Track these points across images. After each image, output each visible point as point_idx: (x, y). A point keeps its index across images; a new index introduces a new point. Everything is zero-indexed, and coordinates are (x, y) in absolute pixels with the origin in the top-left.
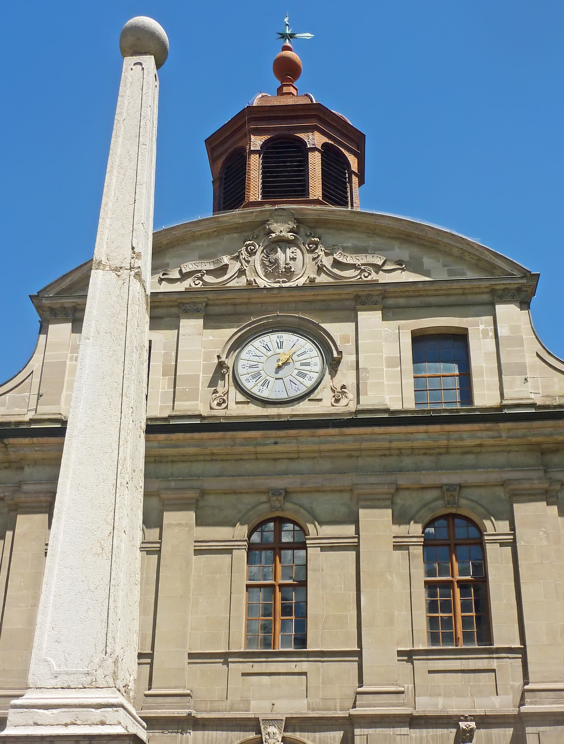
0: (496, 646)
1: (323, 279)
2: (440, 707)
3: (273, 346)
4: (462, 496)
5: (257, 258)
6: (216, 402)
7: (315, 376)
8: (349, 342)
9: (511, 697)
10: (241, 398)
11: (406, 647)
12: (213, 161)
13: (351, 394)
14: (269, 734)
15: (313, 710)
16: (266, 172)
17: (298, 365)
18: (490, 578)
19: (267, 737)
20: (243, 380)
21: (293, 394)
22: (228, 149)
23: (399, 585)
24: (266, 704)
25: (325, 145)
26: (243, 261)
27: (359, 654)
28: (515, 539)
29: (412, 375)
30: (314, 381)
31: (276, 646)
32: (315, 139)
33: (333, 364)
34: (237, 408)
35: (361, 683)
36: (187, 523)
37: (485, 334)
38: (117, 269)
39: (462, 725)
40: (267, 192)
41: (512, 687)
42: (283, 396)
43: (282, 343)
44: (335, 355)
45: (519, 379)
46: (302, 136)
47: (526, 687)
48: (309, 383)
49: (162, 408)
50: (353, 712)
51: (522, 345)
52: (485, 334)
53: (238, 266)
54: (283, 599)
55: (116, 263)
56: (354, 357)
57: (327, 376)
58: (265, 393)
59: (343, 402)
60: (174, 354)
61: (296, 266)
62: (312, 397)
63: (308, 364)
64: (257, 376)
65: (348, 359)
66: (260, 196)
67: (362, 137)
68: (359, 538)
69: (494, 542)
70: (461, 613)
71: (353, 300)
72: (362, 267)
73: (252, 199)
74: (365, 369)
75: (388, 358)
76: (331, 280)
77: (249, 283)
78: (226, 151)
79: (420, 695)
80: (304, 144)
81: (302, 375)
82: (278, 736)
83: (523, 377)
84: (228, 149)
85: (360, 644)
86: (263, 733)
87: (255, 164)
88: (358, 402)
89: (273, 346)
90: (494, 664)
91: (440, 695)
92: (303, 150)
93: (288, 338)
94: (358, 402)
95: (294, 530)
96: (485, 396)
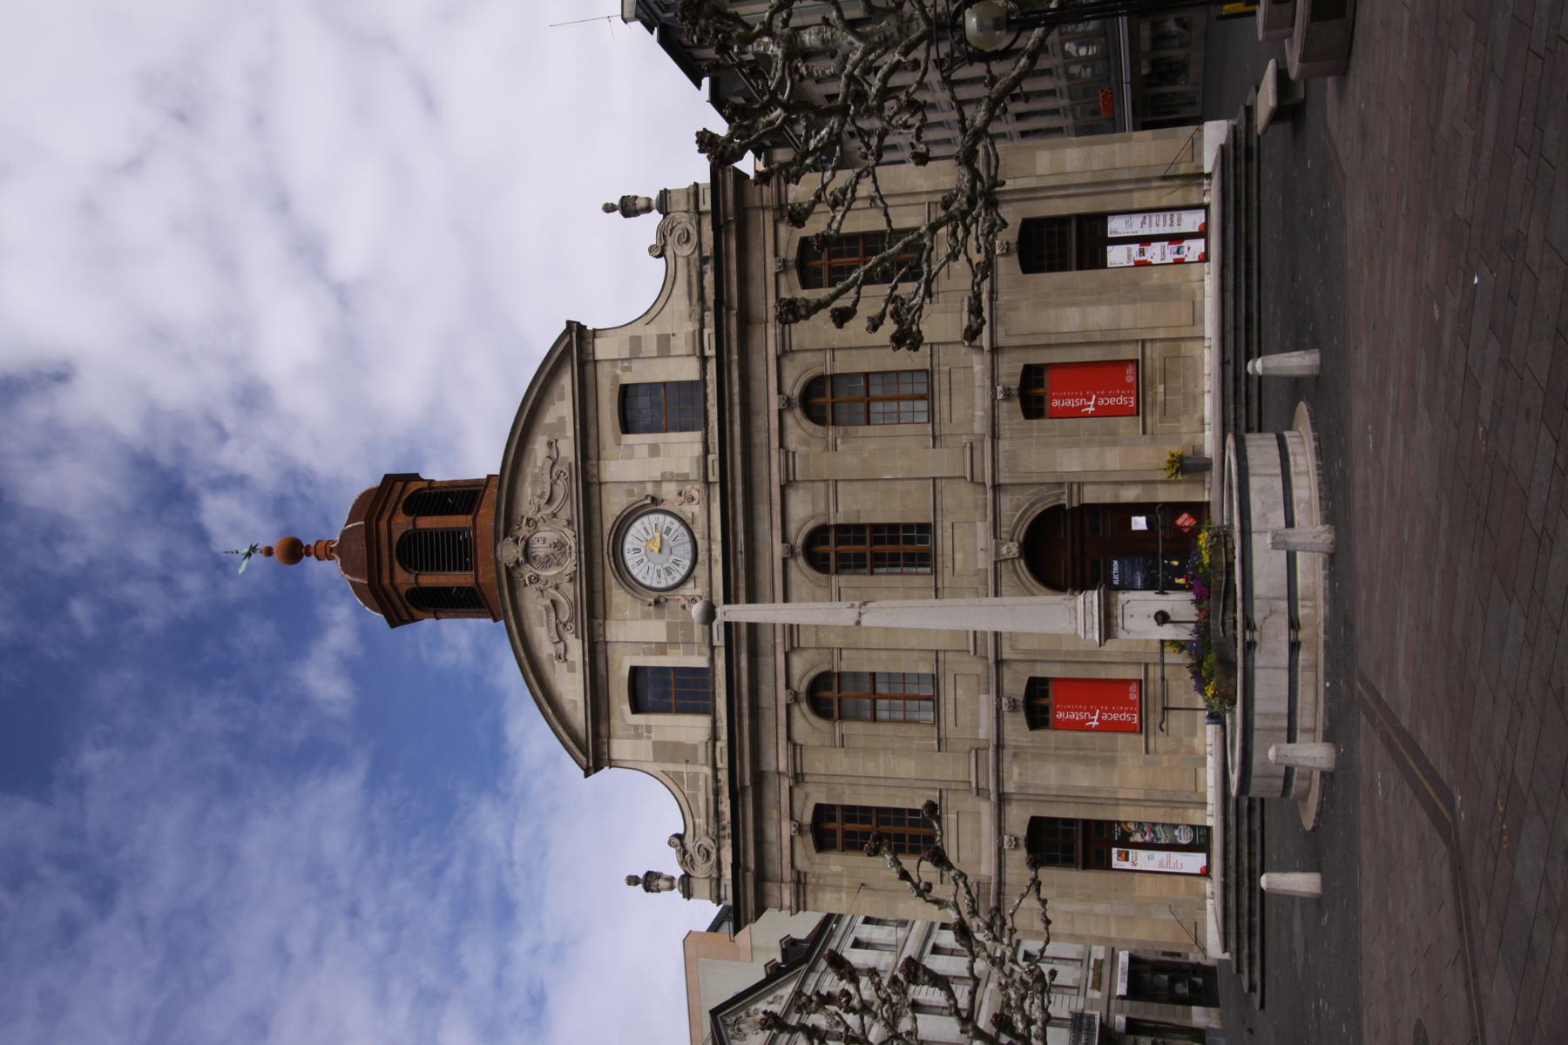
3: (638, 557)
4: (1192, 626)
5: (544, 574)
7: (669, 519)
10: (690, 585)
16: (440, 567)
21: (687, 538)
27: (1144, 341)
32: (402, 523)
33: (654, 504)
37: (629, 369)
38: (1044, 902)
39: (1000, 396)
42: (689, 547)
46: (396, 536)
51: (639, 338)
53: (552, 591)
55: (1038, 905)
58: (687, 563)
59: (695, 494)
61: (552, 537)
64: (668, 571)
71: (588, 485)
76: (608, 525)
77: (571, 580)
87: (429, 580)
89: (638, 557)
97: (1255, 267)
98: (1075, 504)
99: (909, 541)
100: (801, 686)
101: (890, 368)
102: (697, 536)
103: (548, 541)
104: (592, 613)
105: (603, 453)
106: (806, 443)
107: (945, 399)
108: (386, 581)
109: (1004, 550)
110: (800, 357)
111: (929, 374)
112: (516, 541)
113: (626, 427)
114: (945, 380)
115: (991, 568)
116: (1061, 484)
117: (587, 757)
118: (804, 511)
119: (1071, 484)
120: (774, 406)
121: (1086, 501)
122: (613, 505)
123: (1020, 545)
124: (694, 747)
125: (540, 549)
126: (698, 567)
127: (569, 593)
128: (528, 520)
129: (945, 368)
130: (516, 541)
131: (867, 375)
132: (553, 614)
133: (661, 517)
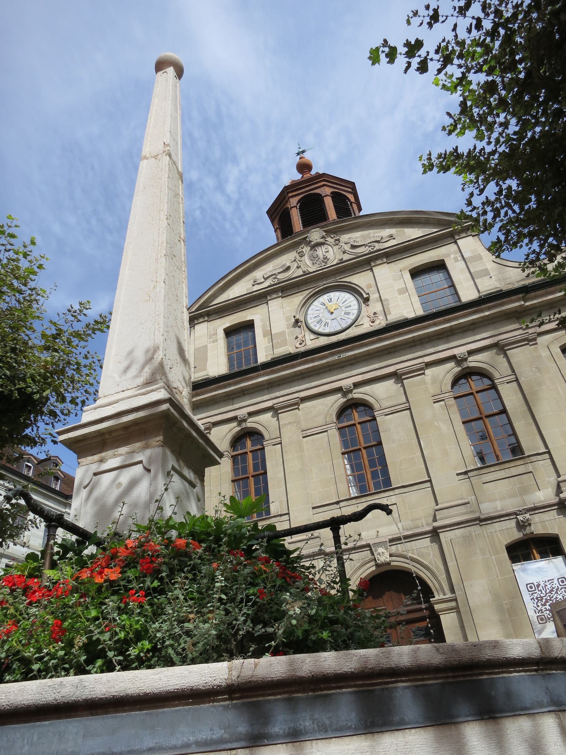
0: (526, 454)
1: (346, 257)
2: (499, 508)
5: (306, 258)
6: (298, 343)
8: (372, 287)
9: (550, 489)
10: (313, 336)
11: (462, 470)
12: (272, 221)
13: (381, 317)
14: (379, 554)
15: (407, 530)
17: (343, 308)
18: (507, 408)
19: (379, 556)
20: (312, 326)
21: (344, 326)
22: (279, 212)
23: (445, 428)
24: (373, 533)
25: (332, 193)
26: (298, 262)
27: (430, 481)
28: (516, 378)
29: (416, 296)
30: (355, 315)
31: (371, 490)
32: (326, 191)
34: (311, 343)
35: (437, 503)
36: (295, 421)
37: (456, 260)
39: (520, 518)
40: (305, 226)
41: (549, 482)
42: (339, 328)
43: (331, 299)
44: (365, 296)
45: (486, 278)
47: (559, 479)
48: (352, 317)
49: (267, 356)
50: (436, 524)
51: (482, 259)
52: (456, 260)
54: (368, 457)
56: (377, 295)
57: (363, 305)
58: (327, 330)
59: (377, 322)
60: (268, 323)
62: (356, 324)
63: (350, 306)
64: (320, 322)
65: (374, 297)
66: (302, 227)
67: (353, 184)
68: (409, 402)
69: (502, 383)
70: (497, 440)
71: (366, 263)
72: (369, 245)
73: (297, 230)
74: (386, 300)
75: (398, 290)
77: (304, 272)
78: (278, 214)
79: (482, 503)
80: (321, 195)
81: (348, 314)
82: (386, 554)
83: (489, 276)
84: (279, 212)
85: (429, 476)
86: (375, 554)
88: (387, 320)
89: (326, 302)
90: (530, 468)
91: (496, 500)
92: (319, 199)
93: (334, 295)
94: (387, 320)
95: (365, 410)
96: (468, 294)
97: (453, 528)
98: (437, 607)
99: (374, 475)
100: (251, 423)
101: (516, 425)
102: (348, 331)
103: (327, 254)
104: (285, 289)
105: (393, 264)
106: (434, 381)
107: (502, 474)
108: (290, 195)
109: (381, 550)
110: (501, 359)
111: (517, 450)
112: (323, 237)
113: (416, 273)
114: (521, 469)
115: (364, 543)
116: (452, 590)
117: (196, 311)
118: (382, 394)
119: (455, 600)
120: (456, 352)
121: (442, 617)
122: (360, 279)
123: (388, 564)
124: (205, 369)
125: (320, 252)
126: (326, 338)
127: (295, 273)
128: (338, 240)
129: (530, 468)
130: (323, 237)
131: (504, 411)
132: (281, 270)
133: (356, 307)
